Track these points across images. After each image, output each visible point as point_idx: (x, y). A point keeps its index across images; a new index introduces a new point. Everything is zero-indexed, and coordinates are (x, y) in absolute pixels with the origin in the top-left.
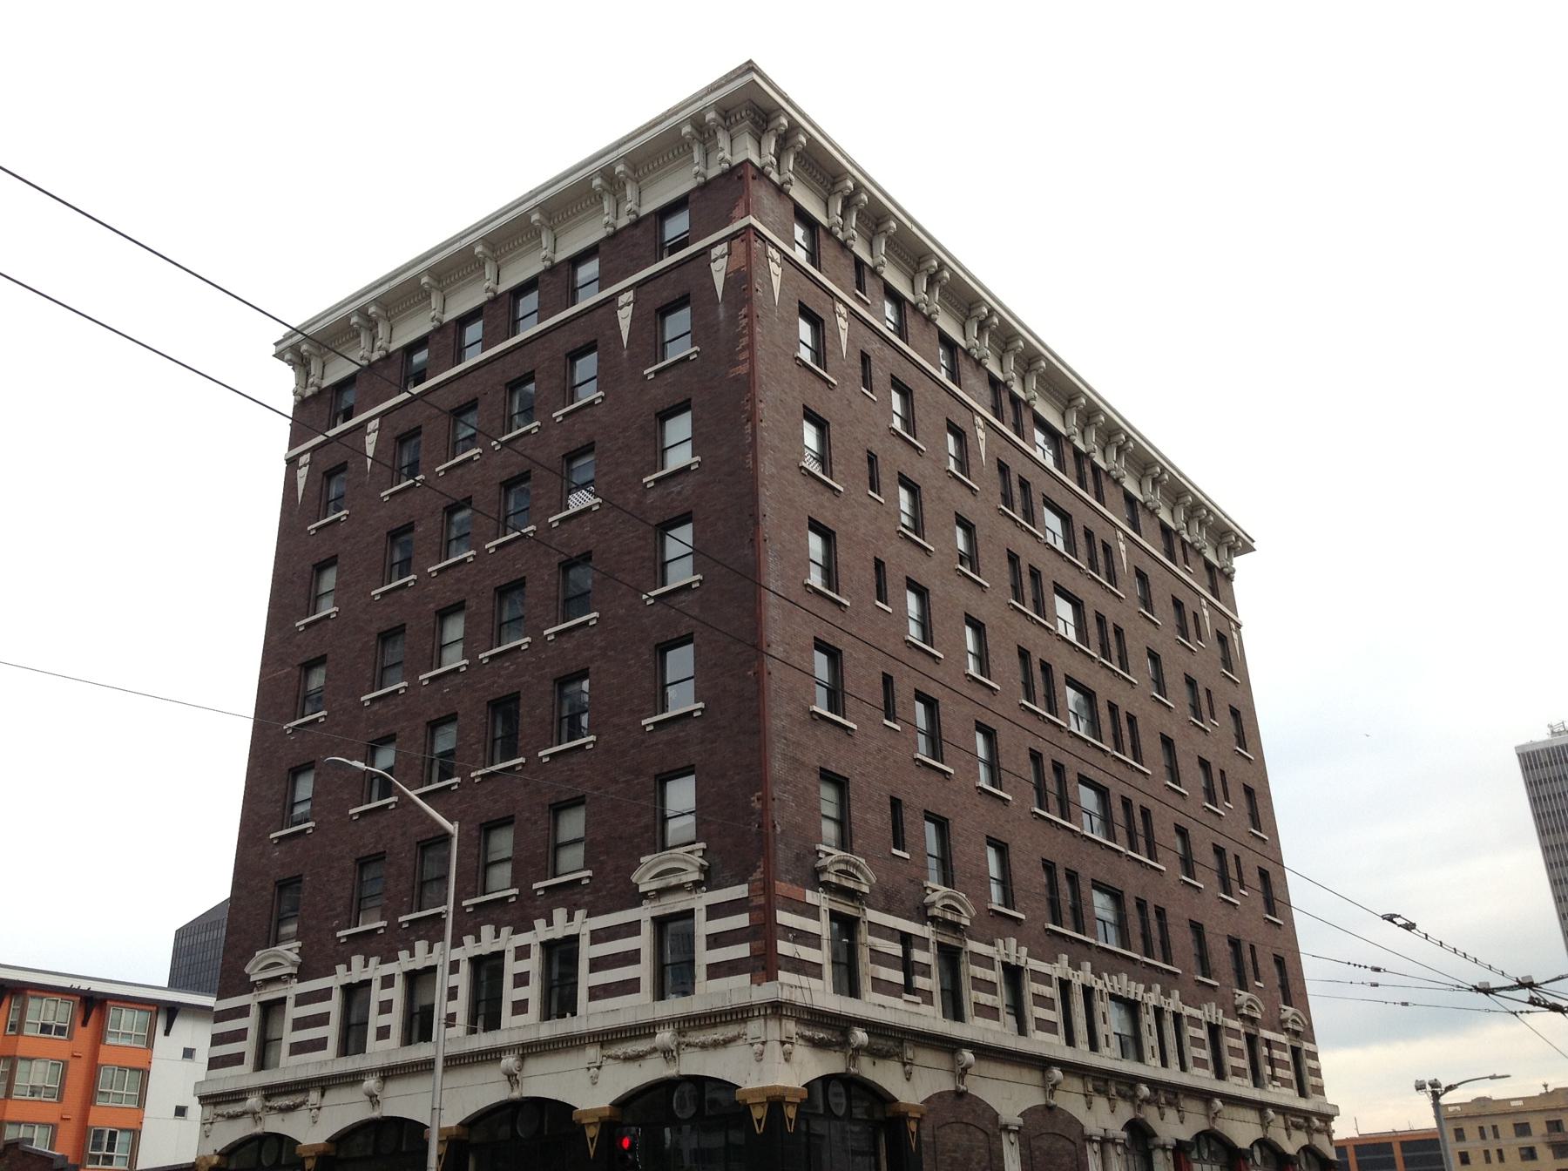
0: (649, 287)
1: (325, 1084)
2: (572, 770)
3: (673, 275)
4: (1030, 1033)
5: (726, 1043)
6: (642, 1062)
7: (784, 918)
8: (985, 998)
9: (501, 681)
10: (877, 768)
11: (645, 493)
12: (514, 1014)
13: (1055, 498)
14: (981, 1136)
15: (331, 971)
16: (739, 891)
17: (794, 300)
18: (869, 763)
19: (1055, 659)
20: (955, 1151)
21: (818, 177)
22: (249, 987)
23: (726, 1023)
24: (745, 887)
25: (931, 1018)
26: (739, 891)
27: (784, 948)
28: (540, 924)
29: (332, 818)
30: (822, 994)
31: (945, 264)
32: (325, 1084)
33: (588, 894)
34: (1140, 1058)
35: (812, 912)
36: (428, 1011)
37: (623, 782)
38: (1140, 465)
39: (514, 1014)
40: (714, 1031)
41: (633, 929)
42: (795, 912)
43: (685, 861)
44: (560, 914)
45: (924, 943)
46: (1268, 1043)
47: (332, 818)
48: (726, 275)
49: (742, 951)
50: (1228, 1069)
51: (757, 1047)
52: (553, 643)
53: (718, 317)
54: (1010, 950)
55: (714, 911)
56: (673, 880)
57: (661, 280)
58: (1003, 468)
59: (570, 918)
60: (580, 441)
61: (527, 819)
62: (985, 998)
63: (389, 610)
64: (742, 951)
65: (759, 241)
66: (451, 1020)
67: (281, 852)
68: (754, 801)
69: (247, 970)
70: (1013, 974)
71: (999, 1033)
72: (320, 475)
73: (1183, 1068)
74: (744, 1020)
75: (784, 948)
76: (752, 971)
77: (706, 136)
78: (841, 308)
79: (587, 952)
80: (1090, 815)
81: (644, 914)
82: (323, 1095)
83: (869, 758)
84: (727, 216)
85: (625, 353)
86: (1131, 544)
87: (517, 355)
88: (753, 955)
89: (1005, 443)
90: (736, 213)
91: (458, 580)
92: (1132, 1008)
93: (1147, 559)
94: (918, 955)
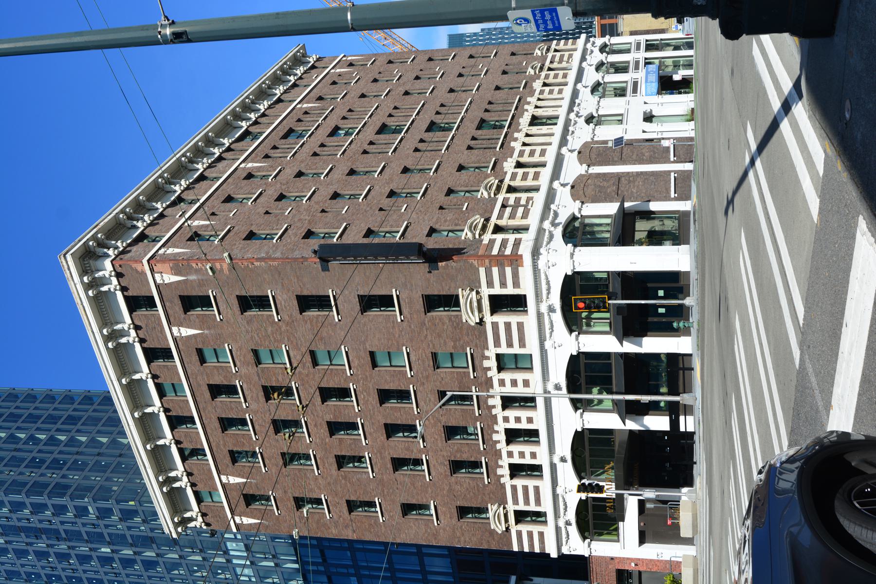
0: (172, 320)
2: (418, 360)
3: (167, 304)
4: (546, 160)
5: (548, 283)
7: (495, 251)
8: (531, 176)
9: (371, 399)
10: (426, 214)
12: (513, 457)
13: (282, 134)
14: (589, 181)
15: (503, 486)
16: (482, 271)
17: (186, 244)
18: (423, 218)
20: (596, 191)
25: (539, 198)
26: (482, 271)
27: (508, 251)
29: (430, 491)
30: (528, 240)
31: (122, 210)
34: (557, 117)
35: (492, 242)
37: (427, 331)
39: (513, 457)
41: (495, 326)
42: (492, 248)
43: (467, 298)
45: (506, 200)
46: (551, 62)
47: (430, 491)
48: (173, 275)
49: (508, 270)
50: (563, 80)
53: (194, 280)
54: (509, 166)
55: (490, 284)
56: (475, 304)
57: (170, 312)
58: (267, 156)
59: (497, 432)
60: (250, 357)
61: (440, 382)
63: (326, 465)
64: (508, 270)
65: (156, 257)
66: (530, 420)
69: (500, 532)
70: (519, 165)
71: (546, 173)
73: (563, 99)
75: (508, 251)
76: (518, 266)
77: (94, 284)
78: (161, 252)
79: (521, 507)
80: (213, 501)
81: (489, 319)
84: (140, 274)
85: (206, 332)
86: (169, 244)
88: (511, 265)
89: (253, 155)
90: (139, 269)
91: (316, 425)
93: (312, 94)
94: (511, 202)
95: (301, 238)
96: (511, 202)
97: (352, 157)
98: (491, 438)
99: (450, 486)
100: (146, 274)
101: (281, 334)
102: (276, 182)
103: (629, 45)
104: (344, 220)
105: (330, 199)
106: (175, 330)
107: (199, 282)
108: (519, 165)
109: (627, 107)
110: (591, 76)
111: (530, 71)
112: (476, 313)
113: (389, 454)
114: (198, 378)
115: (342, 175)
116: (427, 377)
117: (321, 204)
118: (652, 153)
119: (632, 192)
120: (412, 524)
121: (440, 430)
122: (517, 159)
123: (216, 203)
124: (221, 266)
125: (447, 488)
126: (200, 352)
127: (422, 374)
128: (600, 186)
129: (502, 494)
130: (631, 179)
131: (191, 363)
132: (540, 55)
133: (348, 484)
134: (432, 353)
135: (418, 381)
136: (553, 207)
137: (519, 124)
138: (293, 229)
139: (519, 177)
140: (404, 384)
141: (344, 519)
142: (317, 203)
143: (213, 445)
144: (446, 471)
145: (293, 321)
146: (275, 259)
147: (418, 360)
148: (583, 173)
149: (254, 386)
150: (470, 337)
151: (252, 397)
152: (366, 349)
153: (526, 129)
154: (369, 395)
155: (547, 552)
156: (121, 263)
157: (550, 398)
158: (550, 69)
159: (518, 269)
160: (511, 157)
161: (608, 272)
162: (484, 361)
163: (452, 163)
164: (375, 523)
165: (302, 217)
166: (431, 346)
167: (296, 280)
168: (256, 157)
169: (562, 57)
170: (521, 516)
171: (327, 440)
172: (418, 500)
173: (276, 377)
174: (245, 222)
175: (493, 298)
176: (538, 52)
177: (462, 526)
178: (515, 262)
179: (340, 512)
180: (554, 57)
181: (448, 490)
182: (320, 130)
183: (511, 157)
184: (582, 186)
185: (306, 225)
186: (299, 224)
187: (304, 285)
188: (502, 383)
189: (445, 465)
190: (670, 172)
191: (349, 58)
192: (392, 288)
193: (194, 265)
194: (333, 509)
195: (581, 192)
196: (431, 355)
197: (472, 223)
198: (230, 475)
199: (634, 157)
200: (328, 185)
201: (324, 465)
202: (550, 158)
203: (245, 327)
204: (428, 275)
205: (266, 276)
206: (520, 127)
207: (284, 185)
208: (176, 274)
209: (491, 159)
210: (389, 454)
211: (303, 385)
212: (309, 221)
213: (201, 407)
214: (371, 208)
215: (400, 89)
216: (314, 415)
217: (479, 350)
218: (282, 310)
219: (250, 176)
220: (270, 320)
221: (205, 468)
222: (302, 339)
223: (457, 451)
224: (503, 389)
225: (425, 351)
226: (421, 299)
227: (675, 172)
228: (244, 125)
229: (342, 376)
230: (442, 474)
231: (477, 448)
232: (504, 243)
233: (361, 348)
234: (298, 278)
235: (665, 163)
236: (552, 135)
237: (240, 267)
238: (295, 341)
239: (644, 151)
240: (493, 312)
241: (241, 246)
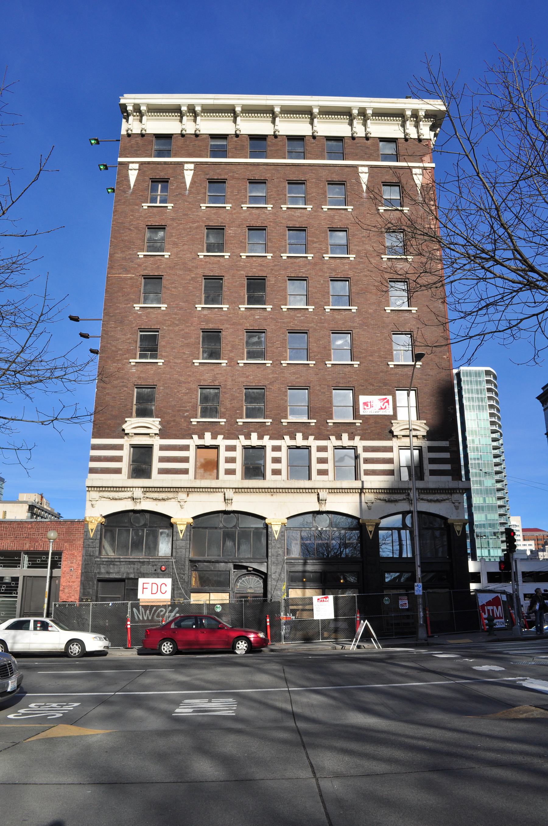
1: (189, 490)
6: (396, 503)
22: (123, 434)
23: (441, 493)
24: (448, 442)
28: (195, 437)
32: (189, 490)
33: (359, 430)
36: (150, 464)
37: (377, 386)
40: (434, 496)
41: (120, 447)
51: (182, 503)
52: (329, 313)
61: (320, 391)
63: (211, 266)
64: (448, 467)
67: (137, 370)
68: (449, 409)
74: (451, 494)
81: (125, 442)
82: (188, 496)
87: (294, 169)
99: (185, 383)
106: (136, 166)
125: (182, 379)
133: (186, 282)
135: (319, 370)
143: (233, 167)
144: (205, 380)
162: (210, 433)
175: (149, 448)
181: (179, 380)
188: (232, 448)
189: (213, 381)
192: (423, 363)
198: (194, 173)
201: (210, 263)
210: (227, 328)
213: (279, 168)
233: (355, 324)
240: (133, 446)
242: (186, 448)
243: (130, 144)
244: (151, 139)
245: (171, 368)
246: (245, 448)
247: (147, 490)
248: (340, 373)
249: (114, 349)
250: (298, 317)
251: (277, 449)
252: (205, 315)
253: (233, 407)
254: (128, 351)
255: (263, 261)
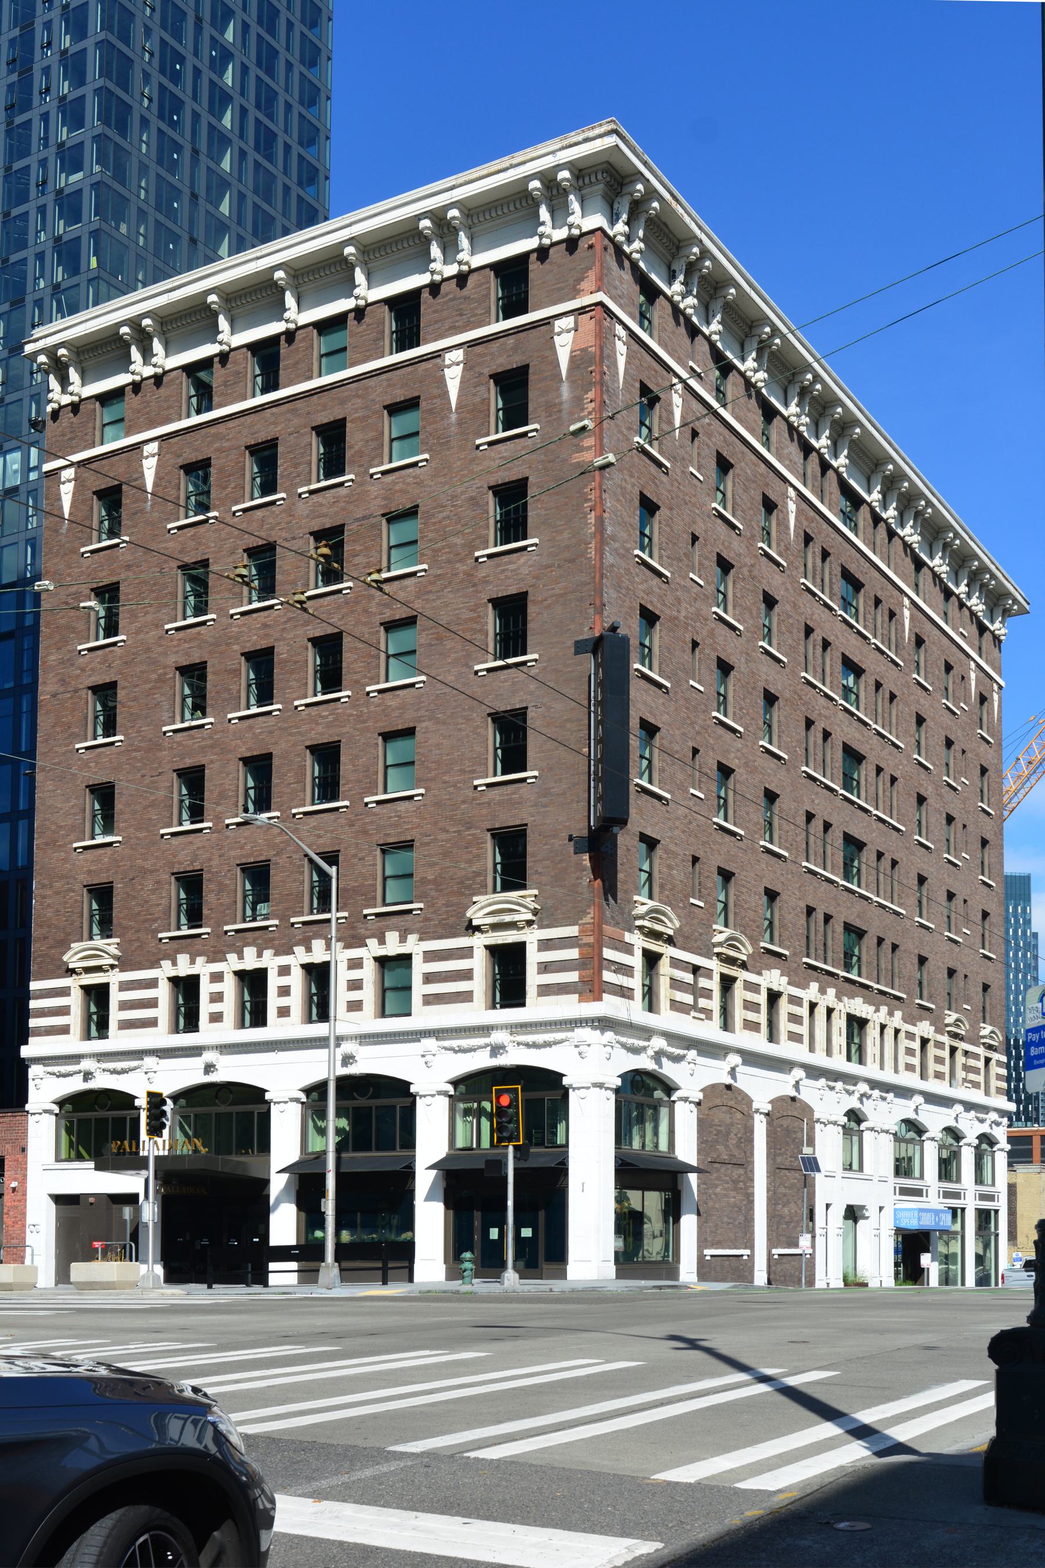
0: (478, 349)
2: (399, 816)
3: (511, 341)
7: (608, 954)
8: (752, 1016)
10: (684, 832)
11: (476, 567)
13: (852, 568)
14: (739, 1115)
15: (155, 964)
16: (572, 931)
18: (677, 828)
19: (836, 727)
21: (665, 241)
25: (710, 1031)
26: (572, 931)
27: (608, 976)
30: (634, 1011)
35: (628, 949)
38: (820, 404)
41: (467, 953)
42: (616, 949)
44: (392, 937)
45: (708, 973)
46: (966, 1053)
48: (572, 352)
49: (573, 977)
50: (931, 1072)
53: (560, 396)
54: (774, 978)
56: (507, 918)
57: (495, 346)
58: (808, 539)
60: (403, 503)
61: (355, 856)
62: (752, 1016)
63: (187, 645)
64: (573, 977)
65: (609, 319)
66: (284, 1012)
70: (774, 997)
71: (758, 1042)
72: (89, 494)
73: (896, 1071)
75: (608, 976)
76: (580, 994)
78: (619, 330)
79: (116, 997)
81: (478, 942)
83: (677, 823)
85: (454, 417)
86: (636, 347)
88: (582, 981)
89: (812, 513)
91: (265, 626)
92: (862, 1023)
93: (929, 626)
95: (643, 603)
96: (703, 982)
97: (801, 699)
98: (248, 945)
99: (151, 872)
100: (574, 298)
101: (449, 562)
102: (756, 556)
103: (990, 1182)
104: (677, 683)
105: (718, 658)
106: (458, 355)
107: (555, 405)
108: (924, 1042)
109: (876, 1179)
110: (935, 1120)
111: (951, 1017)
112: (490, 920)
113: (212, 762)
114: (359, 401)
115: (766, 680)
116: (365, 832)
117: (709, 641)
118: (788, 1219)
119: (717, 1186)
120: (73, 802)
121: (261, 855)
122: (903, 1030)
123: (715, 440)
124: (589, 448)
125: (148, 865)
126: (411, 404)
127: (372, 822)
128: (728, 1133)
129: (140, 963)
130: (741, 1185)
131: (389, 386)
132: (714, 940)
134: (413, 841)
136: (692, 1054)
137: (852, 997)
138: (660, 588)
139: (751, 996)
140: (350, 790)
141: (78, 676)
142: (712, 633)
144: (180, 863)
145: (474, 585)
146: (600, 552)
147: (399, 816)
148: (755, 1106)
149: (344, 509)
150: (444, 909)
151: (321, 505)
152: (420, 721)
153: (842, 1008)
154: (329, 726)
155: (31, 1039)
156: (598, 248)
157: (327, 1046)
158: (953, 1050)
159: (575, 993)
160: (789, 983)
161: (567, 1145)
162: (397, 934)
163: (783, 879)
164: (73, 734)
165: (684, 605)
166: (426, 839)
167: (557, 592)
168: (807, 519)
169: (976, 1071)
170: (98, 995)
171: (235, 647)
172: (122, 813)
173: (361, 551)
174: (678, 497)
176: (986, 1030)
177: (73, 891)
178: (587, 987)
179: (92, 670)
180: (976, 1057)
182: (855, 640)
183: (789, 983)
184: (731, 1103)
185: (667, 612)
186: (669, 599)
187: (548, 607)
189: (192, 863)
190: (752, 1247)
191: (996, 696)
192: (541, 770)
193: (591, 395)
194: (97, 657)
195: (718, 1102)
196: (409, 838)
197: (664, 914)
199: (782, 1190)
200: (747, 654)
202: (785, 1049)
203: (462, 493)
204: (565, 835)
205: (566, 535)
206: (845, 999)
207: (750, 571)
208: (572, 359)
209: (787, 948)
210: (212, 762)
211: (347, 603)
212: (676, 618)
213: (299, 404)
214: (698, 733)
215: (930, 789)
216: (286, 623)
217: (419, 925)
218: (498, 565)
219: (770, 506)
220: (478, 542)
221: (172, 411)
222: (438, 602)
223: (220, 884)
224: (342, 967)
225: (417, 827)
226: (518, 823)
227: (751, 1257)
228: (874, 497)
229: (365, 676)
230: (175, 856)
231: (227, 919)
232: (626, 970)
233: (422, 712)
234: (561, 595)
235: (769, 1239)
236: (829, 1052)
237: (586, 486)
238: (435, 589)
239: (792, 1205)
241: (629, 487)
242: (153, 984)
243: (61, 429)
244: (92, 407)
245: (132, 849)
246: (172, 980)
247: (101, 1057)
248: (391, 817)
249: (53, 827)
250: (323, 717)
251: (217, 977)
252: (179, 743)
253: (221, 904)
254: (73, 828)
255: (268, 616)
